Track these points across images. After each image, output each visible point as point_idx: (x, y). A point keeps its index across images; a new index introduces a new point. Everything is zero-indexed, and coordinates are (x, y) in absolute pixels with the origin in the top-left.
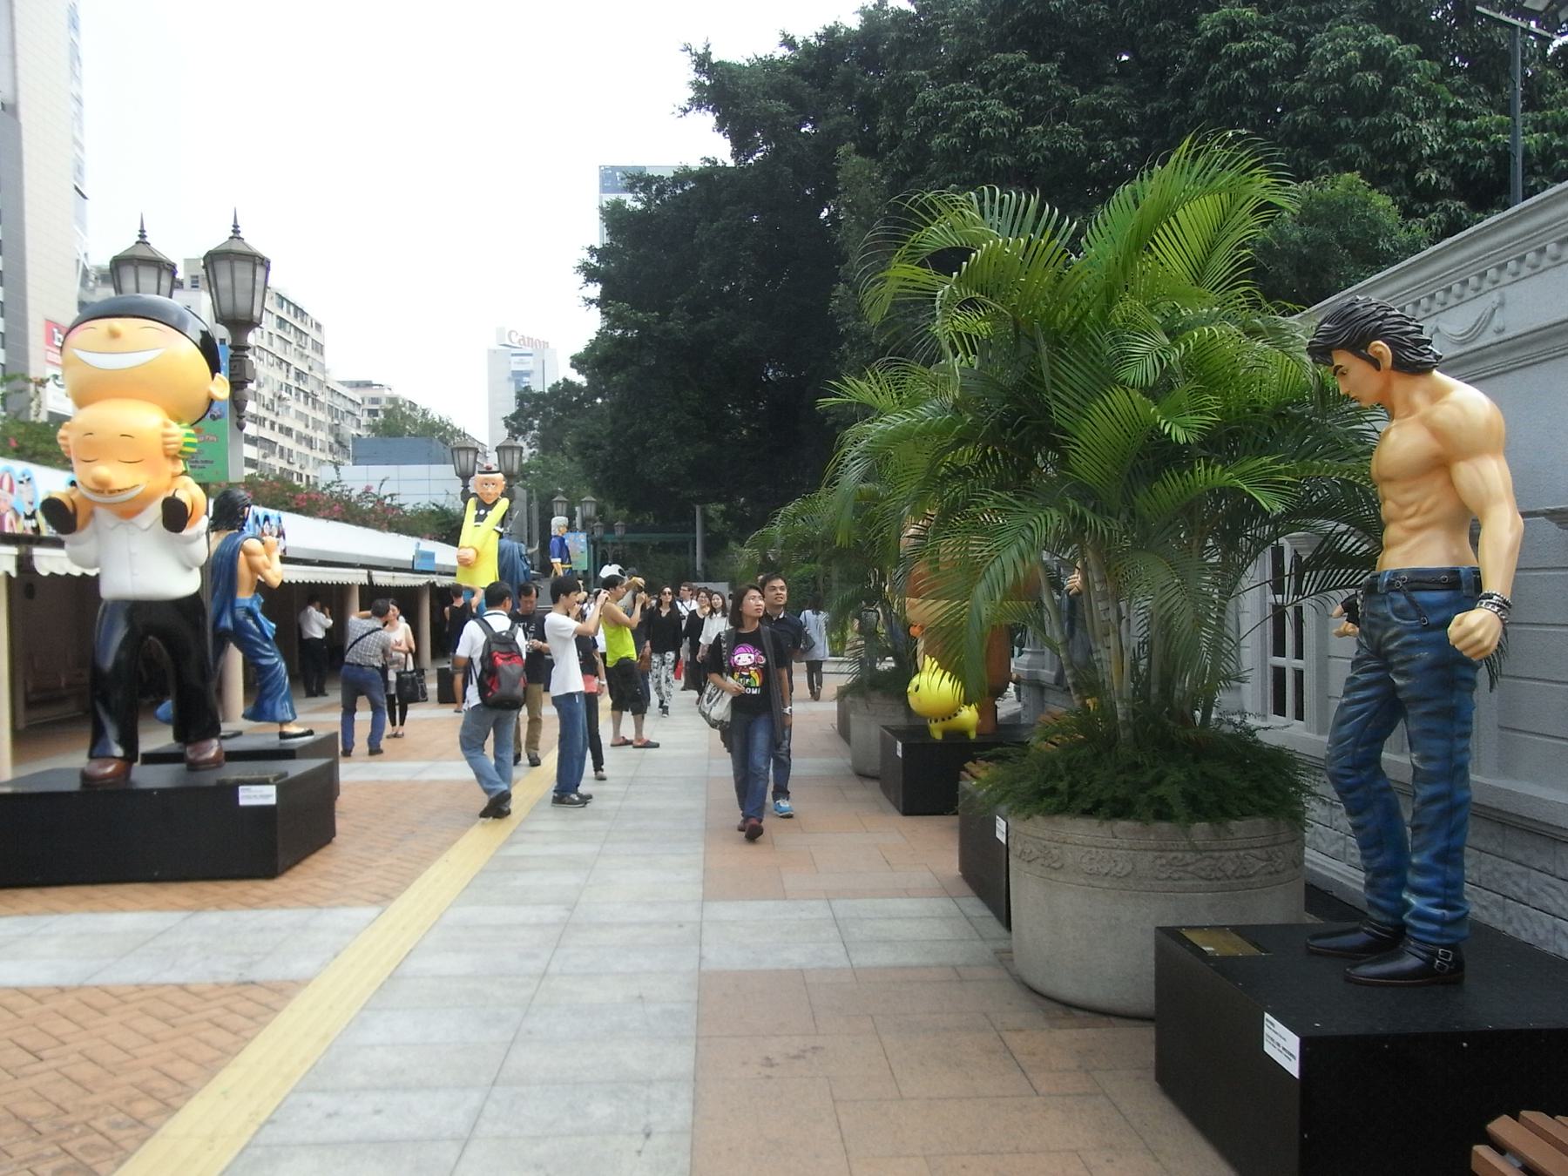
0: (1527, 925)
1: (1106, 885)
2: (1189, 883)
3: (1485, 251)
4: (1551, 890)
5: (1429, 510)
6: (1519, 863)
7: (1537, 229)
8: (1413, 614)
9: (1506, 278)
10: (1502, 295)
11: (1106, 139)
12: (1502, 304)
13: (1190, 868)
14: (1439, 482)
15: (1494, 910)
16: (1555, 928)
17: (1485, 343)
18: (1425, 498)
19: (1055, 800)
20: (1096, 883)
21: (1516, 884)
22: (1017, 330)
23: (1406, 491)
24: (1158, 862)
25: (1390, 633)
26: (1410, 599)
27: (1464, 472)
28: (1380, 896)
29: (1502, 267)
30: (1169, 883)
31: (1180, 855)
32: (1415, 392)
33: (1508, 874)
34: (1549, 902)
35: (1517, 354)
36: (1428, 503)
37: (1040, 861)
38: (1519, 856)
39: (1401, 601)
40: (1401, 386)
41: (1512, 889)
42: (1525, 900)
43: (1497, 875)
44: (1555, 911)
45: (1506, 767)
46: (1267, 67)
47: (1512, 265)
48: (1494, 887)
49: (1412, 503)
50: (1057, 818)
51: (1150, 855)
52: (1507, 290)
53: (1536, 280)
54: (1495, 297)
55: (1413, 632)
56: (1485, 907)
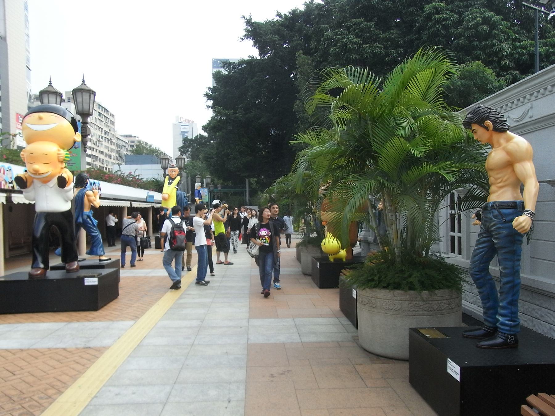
0: (541, 327)
1: (391, 313)
2: (421, 312)
3: (526, 89)
4: (549, 315)
5: (506, 181)
6: (538, 305)
7: (544, 81)
8: (500, 217)
9: (533, 98)
10: (532, 104)
11: (391, 49)
12: (532, 108)
13: (421, 307)
14: (509, 170)
15: (529, 322)
16: (551, 328)
17: (526, 121)
18: (504, 176)
19: (373, 283)
20: (388, 312)
21: (537, 313)
22: (360, 117)
23: (498, 174)
24: (410, 305)
25: (492, 224)
26: (499, 212)
27: (518, 167)
28: (489, 317)
29: (532, 95)
30: (414, 312)
31: (418, 302)
32: (501, 139)
33: (534, 309)
34: (548, 319)
35: (537, 125)
36: (505, 178)
37: (368, 304)
38: (538, 303)
39: (496, 212)
40: (496, 136)
41: (535, 314)
42: (540, 318)
43: (530, 309)
44: (550, 322)
45: (533, 271)
46: (448, 24)
47: (535, 94)
48: (529, 314)
49: (500, 178)
50: (374, 289)
51: (407, 303)
52: (533, 103)
53: (544, 99)
54: (529, 105)
55: (500, 224)
56: (526, 321)
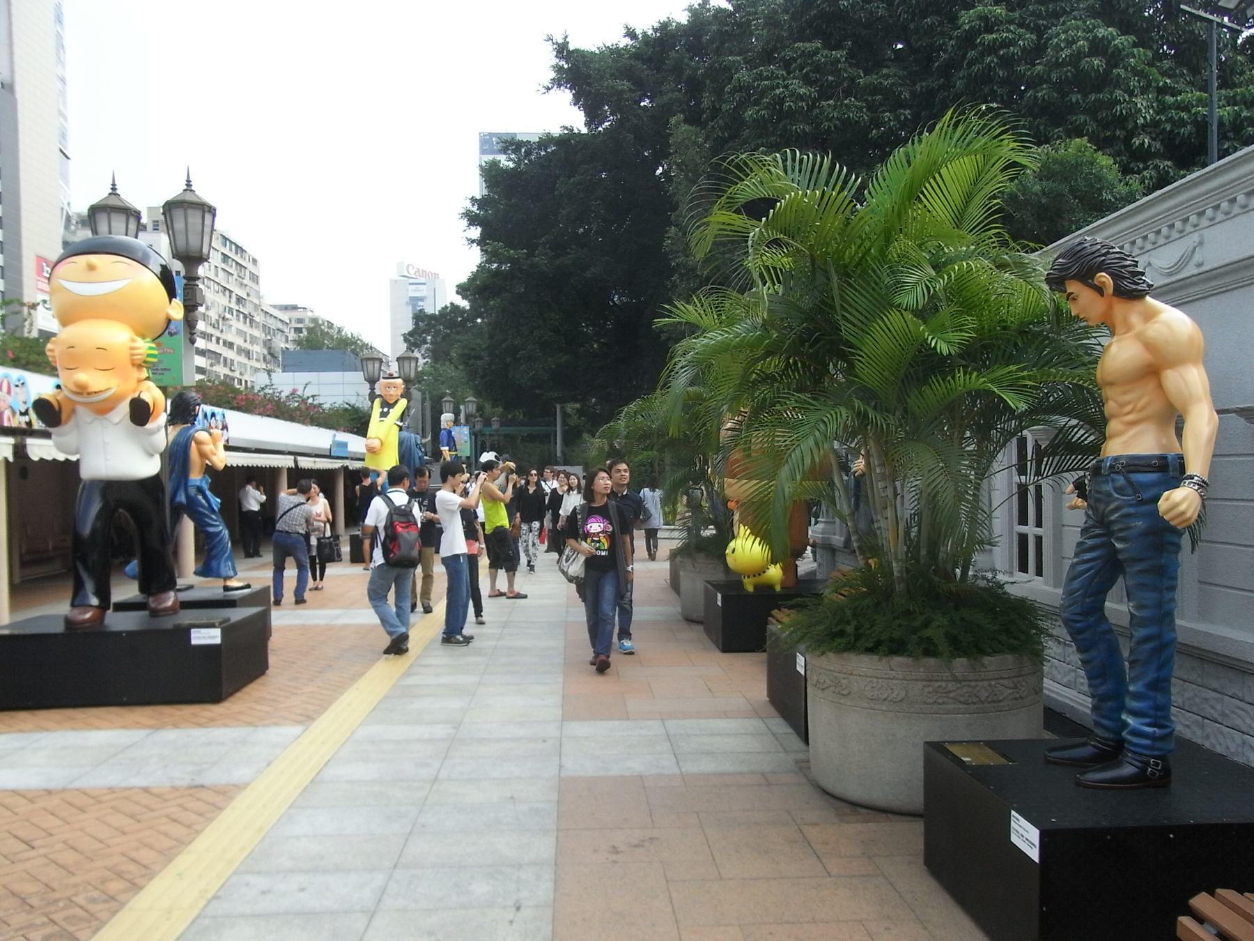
0: (1221, 740)
1: (884, 708)
2: (951, 707)
3: (1188, 201)
4: (1240, 712)
5: (1143, 408)
6: (1215, 690)
7: (1229, 183)
8: (1130, 491)
9: (1204, 222)
10: (1201, 236)
11: (884, 112)
12: (1201, 243)
13: (952, 695)
14: (1151, 386)
15: (1195, 728)
16: (1244, 743)
17: (1188, 274)
18: (1140, 399)
19: (844, 640)
20: (877, 707)
21: (1213, 707)
22: (813, 264)
23: (1125, 393)
24: (926, 690)
25: (1112, 506)
26: (1127, 480)
27: (1171, 378)
28: (1104, 717)
29: (1201, 214)
30: (935, 707)
31: (944, 684)
32: (1131, 313)
33: (1206, 700)
34: (1238, 722)
35: (1214, 283)
36: (1142, 403)
37: (832, 689)
38: (1215, 685)
39: (1121, 481)
40: (1121, 309)
41: (1209, 711)
42: (1220, 720)
43: (1197, 700)
44: (1243, 729)
45: (1204, 614)
46: (1013, 54)
47: (1209, 212)
48: (1195, 709)
49: (1129, 403)
50: (845, 654)
51: (920, 684)
52: (1205, 232)
53: (1228, 224)
54: (1195, 237)
55: (1130, 506)
56: (1187, 726)
